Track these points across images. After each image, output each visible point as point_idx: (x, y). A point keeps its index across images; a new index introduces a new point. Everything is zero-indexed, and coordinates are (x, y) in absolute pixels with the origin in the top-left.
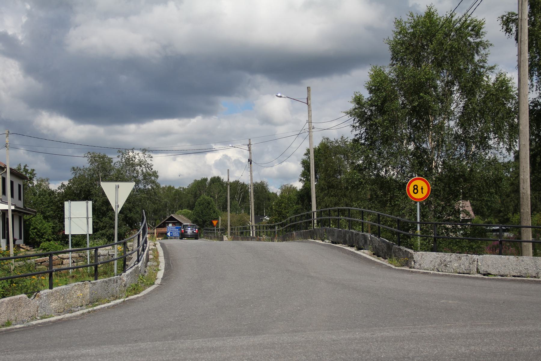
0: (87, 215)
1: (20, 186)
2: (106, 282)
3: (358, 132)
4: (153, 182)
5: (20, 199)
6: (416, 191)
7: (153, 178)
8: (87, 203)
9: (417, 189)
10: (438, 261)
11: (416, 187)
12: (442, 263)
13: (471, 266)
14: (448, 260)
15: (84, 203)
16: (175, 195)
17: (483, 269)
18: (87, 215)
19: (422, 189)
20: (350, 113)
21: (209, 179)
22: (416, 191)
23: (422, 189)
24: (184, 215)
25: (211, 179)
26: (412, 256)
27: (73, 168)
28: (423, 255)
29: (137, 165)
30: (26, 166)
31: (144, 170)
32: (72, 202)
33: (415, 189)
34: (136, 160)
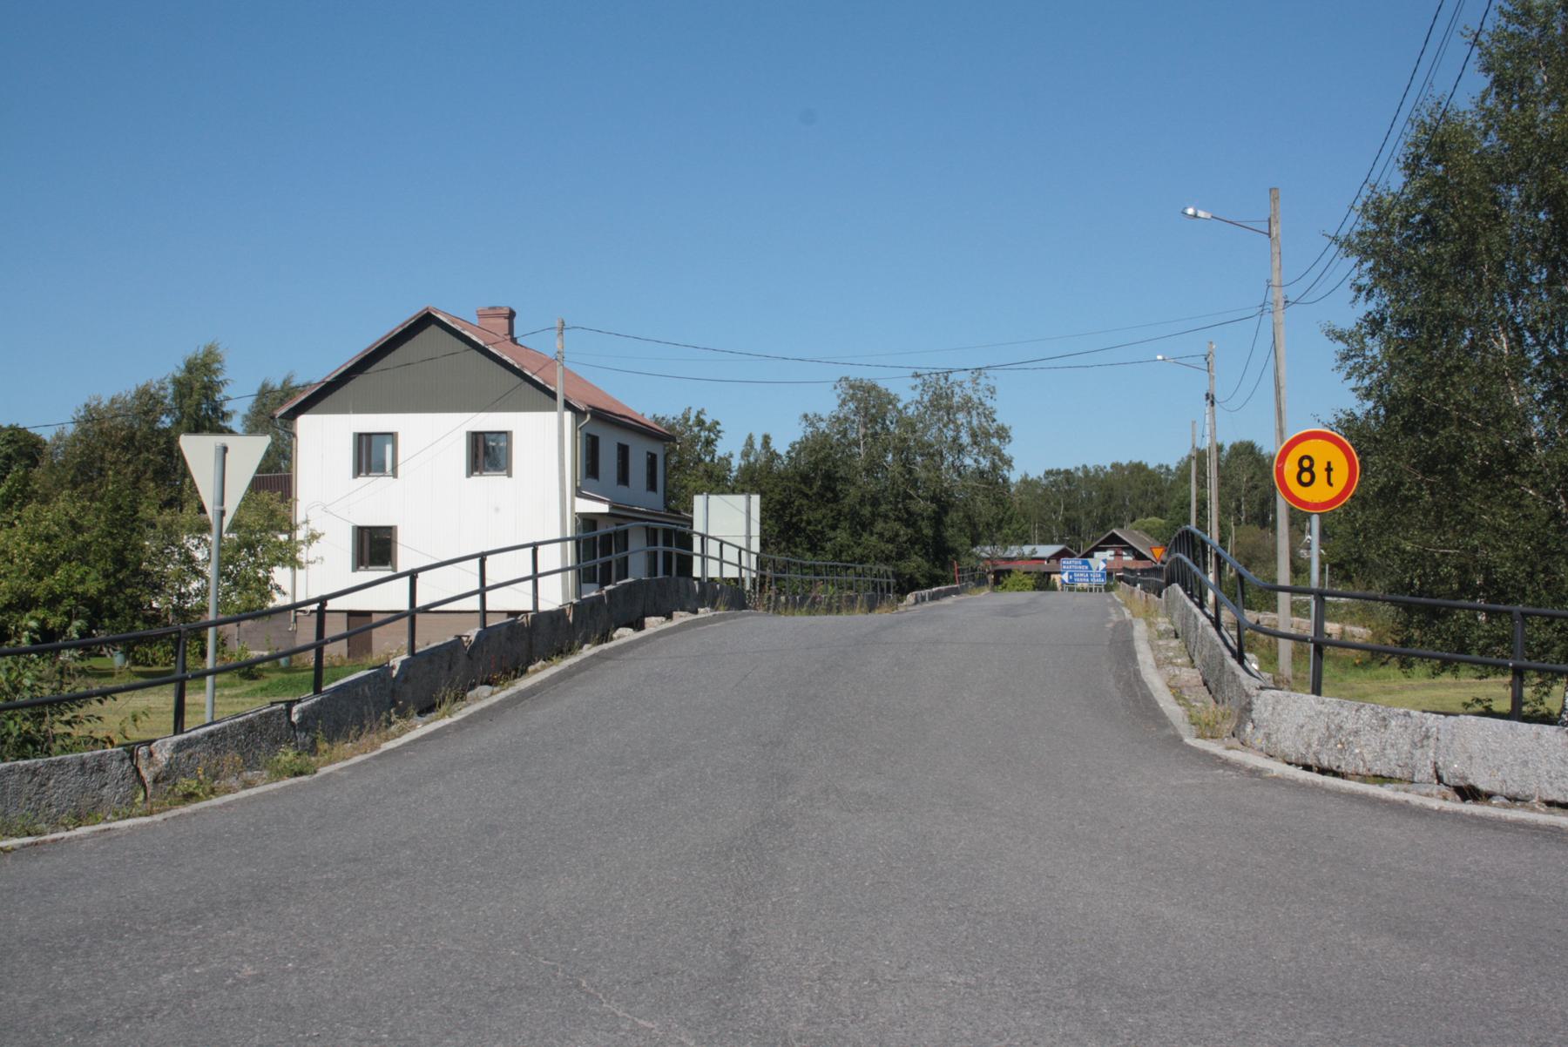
0: (749, 530)
1: (652, 460)
2: (35, 773)
3: (1371, 306)
4: (997, 452)
5: (652, 486)
6: (1306, 477)
7: (995, 441)
8: (749, 500)
9: (1310, 469)
10: (1320, 726)
11: (1306, 463)
12: (1330, 737)
13: (1418, 753)
14: (1349, 726)
15: (740, 499)
16: (1146, 483)
17: (1455, 769)
18: (749, 530)
19: (1329, 469)
20: (1347, 245)
21: (1227, 447)
22: (1306, 477)
23: (1329, 469)
24: (1147, 531)
25: (1233, 447)
26: (1250, 703)
27: (806, 416)
28: (1278, 702)
29: (959, 409)
30: (699, 413)
31: (975, 422)
32: (713, 498)
33: (1302, 470)
34: (956, 399)
